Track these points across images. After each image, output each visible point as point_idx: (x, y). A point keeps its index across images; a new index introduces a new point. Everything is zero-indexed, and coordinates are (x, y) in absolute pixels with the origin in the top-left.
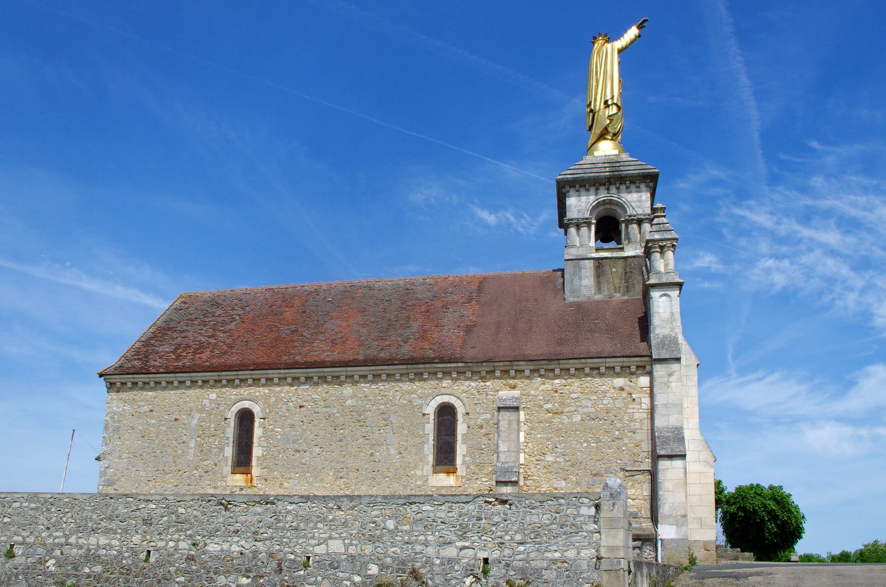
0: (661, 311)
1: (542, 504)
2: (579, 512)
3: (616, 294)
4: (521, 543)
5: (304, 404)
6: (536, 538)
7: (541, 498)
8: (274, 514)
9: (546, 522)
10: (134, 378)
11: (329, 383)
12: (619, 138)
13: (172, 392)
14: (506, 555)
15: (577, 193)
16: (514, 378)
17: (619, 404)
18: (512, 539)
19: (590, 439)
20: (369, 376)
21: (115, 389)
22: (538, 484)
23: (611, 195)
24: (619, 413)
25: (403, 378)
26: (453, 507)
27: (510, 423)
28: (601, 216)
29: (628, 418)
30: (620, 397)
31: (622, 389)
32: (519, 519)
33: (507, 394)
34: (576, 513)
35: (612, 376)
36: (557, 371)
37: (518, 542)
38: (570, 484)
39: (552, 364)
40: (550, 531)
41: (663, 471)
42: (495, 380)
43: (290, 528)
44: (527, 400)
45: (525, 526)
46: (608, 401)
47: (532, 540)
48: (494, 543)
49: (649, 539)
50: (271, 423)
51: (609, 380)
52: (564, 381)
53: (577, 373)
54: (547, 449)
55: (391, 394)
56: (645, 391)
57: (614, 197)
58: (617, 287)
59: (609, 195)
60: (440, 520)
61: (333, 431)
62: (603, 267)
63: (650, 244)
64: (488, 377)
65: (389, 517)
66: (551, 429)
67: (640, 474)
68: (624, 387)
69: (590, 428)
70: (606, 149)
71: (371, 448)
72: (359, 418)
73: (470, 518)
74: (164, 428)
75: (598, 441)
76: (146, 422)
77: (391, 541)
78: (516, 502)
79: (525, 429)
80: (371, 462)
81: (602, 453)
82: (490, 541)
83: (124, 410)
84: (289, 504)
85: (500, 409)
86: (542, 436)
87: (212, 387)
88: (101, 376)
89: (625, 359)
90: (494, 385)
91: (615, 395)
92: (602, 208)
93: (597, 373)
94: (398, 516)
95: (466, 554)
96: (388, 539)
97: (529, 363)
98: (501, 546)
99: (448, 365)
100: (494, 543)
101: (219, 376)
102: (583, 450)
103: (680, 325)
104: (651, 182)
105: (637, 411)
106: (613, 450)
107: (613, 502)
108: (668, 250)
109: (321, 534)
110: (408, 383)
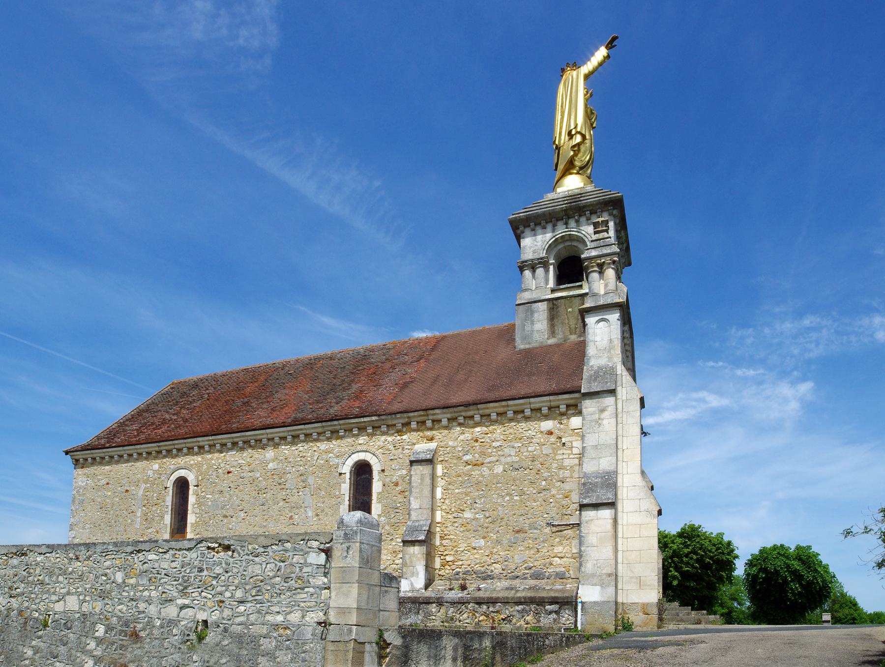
0: (598, 339)
1: (266, 550)
2: (306, 560)
3: (571, 336)
4: (242, 602)
5: (232, 469)
6: (258, 595)
7: (265, 542)
8: (27, 567)
9: (269, 573)
10: (92, 454)
11: (253, 447)
12: (589, 171)
13: (123, 465)
14: (225, 617)
15: (533, 232)
16: (431, 429)
17: (546, 450)
18: (232, 596)
19: (514, 492)
20: (288, 437)
21: (80, 466)
22: (455, 544)
23: (569, 229)
24: (546, 461)
25: (321, 438)
26: (177, 556)
27: (422, 477)
28: (563, 257)
29: (556, 465)
30: (548, 441)
31: (550, 433)
32: (241, 569)
33: (423, 448)
34: (302, 561)
35: (539, 419)
36: (477, 418)
37: (238, 600)
38: (489, 543)
39: (470, 410)
40: (273, 586)
41: (587, 522)
42: (412, 433)
43: (38, 583)
44: (445, 452)
45: (247, 578)
46: (534, 447)
47: (253, 598)
48: (214, 602)
49: (567, 602)
50: (203, 490)
51: (536, 424)
52: (485, 429)
53: (499, 418)
54: (465, 505)
55: (309, 454)
56: (577, 433)
57: (573, 231)
58: (573, 329)
59: (567, 230)
60: (164, 572)
61: (257, 495)
62: (558, 307)
63: (586, 263)
64: (404, 429)
65: (119, 568)
66: (470, 483)
67: (569, 529)
68: (553, 431)
69: (514, 479)
70: (573, 183)
71: (290, 511)
72: (280, 481)
73: (192, 569)
74: (117, 499)
75: (522, 493)
76: (103, 494)
77: (118, 597)
78: (239, 548)
79: (442, 484)
80: (290, 525)
81: (527, 507)
82: (210, 599)
83: (87, 484)
84: (39, 555)
85: (412, 463)
86: (460, 491)
87: (156, 458)
88: (67, 453)
89: (552, 398)
90: (411, 438)
91: (542, 440)
92: (560, 246)
93: (522, 417)
94: (126, 567)
95: (186, 614)
96: (116, 595)
97: (445, 410)
98: (221, 604)
99: (362, 420)
100: (214, 602)
101: (159, 446)
102: (505, 504)
103: (620, 352)
104: (614, 209)
105: (567, 457)
106: (538, 503)
107: (349, 544)
108: (607, 268)
109: (62, 588)
110: (325, 442)
